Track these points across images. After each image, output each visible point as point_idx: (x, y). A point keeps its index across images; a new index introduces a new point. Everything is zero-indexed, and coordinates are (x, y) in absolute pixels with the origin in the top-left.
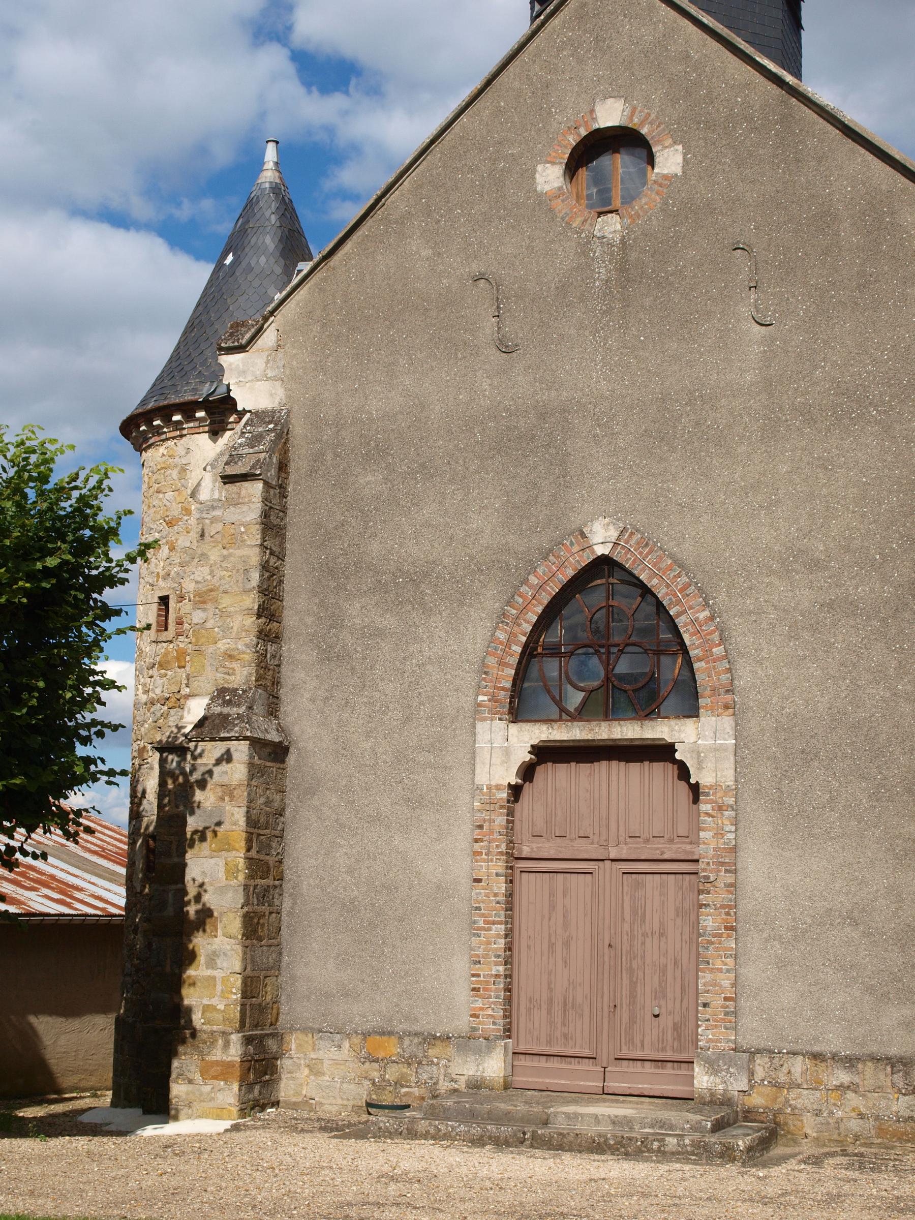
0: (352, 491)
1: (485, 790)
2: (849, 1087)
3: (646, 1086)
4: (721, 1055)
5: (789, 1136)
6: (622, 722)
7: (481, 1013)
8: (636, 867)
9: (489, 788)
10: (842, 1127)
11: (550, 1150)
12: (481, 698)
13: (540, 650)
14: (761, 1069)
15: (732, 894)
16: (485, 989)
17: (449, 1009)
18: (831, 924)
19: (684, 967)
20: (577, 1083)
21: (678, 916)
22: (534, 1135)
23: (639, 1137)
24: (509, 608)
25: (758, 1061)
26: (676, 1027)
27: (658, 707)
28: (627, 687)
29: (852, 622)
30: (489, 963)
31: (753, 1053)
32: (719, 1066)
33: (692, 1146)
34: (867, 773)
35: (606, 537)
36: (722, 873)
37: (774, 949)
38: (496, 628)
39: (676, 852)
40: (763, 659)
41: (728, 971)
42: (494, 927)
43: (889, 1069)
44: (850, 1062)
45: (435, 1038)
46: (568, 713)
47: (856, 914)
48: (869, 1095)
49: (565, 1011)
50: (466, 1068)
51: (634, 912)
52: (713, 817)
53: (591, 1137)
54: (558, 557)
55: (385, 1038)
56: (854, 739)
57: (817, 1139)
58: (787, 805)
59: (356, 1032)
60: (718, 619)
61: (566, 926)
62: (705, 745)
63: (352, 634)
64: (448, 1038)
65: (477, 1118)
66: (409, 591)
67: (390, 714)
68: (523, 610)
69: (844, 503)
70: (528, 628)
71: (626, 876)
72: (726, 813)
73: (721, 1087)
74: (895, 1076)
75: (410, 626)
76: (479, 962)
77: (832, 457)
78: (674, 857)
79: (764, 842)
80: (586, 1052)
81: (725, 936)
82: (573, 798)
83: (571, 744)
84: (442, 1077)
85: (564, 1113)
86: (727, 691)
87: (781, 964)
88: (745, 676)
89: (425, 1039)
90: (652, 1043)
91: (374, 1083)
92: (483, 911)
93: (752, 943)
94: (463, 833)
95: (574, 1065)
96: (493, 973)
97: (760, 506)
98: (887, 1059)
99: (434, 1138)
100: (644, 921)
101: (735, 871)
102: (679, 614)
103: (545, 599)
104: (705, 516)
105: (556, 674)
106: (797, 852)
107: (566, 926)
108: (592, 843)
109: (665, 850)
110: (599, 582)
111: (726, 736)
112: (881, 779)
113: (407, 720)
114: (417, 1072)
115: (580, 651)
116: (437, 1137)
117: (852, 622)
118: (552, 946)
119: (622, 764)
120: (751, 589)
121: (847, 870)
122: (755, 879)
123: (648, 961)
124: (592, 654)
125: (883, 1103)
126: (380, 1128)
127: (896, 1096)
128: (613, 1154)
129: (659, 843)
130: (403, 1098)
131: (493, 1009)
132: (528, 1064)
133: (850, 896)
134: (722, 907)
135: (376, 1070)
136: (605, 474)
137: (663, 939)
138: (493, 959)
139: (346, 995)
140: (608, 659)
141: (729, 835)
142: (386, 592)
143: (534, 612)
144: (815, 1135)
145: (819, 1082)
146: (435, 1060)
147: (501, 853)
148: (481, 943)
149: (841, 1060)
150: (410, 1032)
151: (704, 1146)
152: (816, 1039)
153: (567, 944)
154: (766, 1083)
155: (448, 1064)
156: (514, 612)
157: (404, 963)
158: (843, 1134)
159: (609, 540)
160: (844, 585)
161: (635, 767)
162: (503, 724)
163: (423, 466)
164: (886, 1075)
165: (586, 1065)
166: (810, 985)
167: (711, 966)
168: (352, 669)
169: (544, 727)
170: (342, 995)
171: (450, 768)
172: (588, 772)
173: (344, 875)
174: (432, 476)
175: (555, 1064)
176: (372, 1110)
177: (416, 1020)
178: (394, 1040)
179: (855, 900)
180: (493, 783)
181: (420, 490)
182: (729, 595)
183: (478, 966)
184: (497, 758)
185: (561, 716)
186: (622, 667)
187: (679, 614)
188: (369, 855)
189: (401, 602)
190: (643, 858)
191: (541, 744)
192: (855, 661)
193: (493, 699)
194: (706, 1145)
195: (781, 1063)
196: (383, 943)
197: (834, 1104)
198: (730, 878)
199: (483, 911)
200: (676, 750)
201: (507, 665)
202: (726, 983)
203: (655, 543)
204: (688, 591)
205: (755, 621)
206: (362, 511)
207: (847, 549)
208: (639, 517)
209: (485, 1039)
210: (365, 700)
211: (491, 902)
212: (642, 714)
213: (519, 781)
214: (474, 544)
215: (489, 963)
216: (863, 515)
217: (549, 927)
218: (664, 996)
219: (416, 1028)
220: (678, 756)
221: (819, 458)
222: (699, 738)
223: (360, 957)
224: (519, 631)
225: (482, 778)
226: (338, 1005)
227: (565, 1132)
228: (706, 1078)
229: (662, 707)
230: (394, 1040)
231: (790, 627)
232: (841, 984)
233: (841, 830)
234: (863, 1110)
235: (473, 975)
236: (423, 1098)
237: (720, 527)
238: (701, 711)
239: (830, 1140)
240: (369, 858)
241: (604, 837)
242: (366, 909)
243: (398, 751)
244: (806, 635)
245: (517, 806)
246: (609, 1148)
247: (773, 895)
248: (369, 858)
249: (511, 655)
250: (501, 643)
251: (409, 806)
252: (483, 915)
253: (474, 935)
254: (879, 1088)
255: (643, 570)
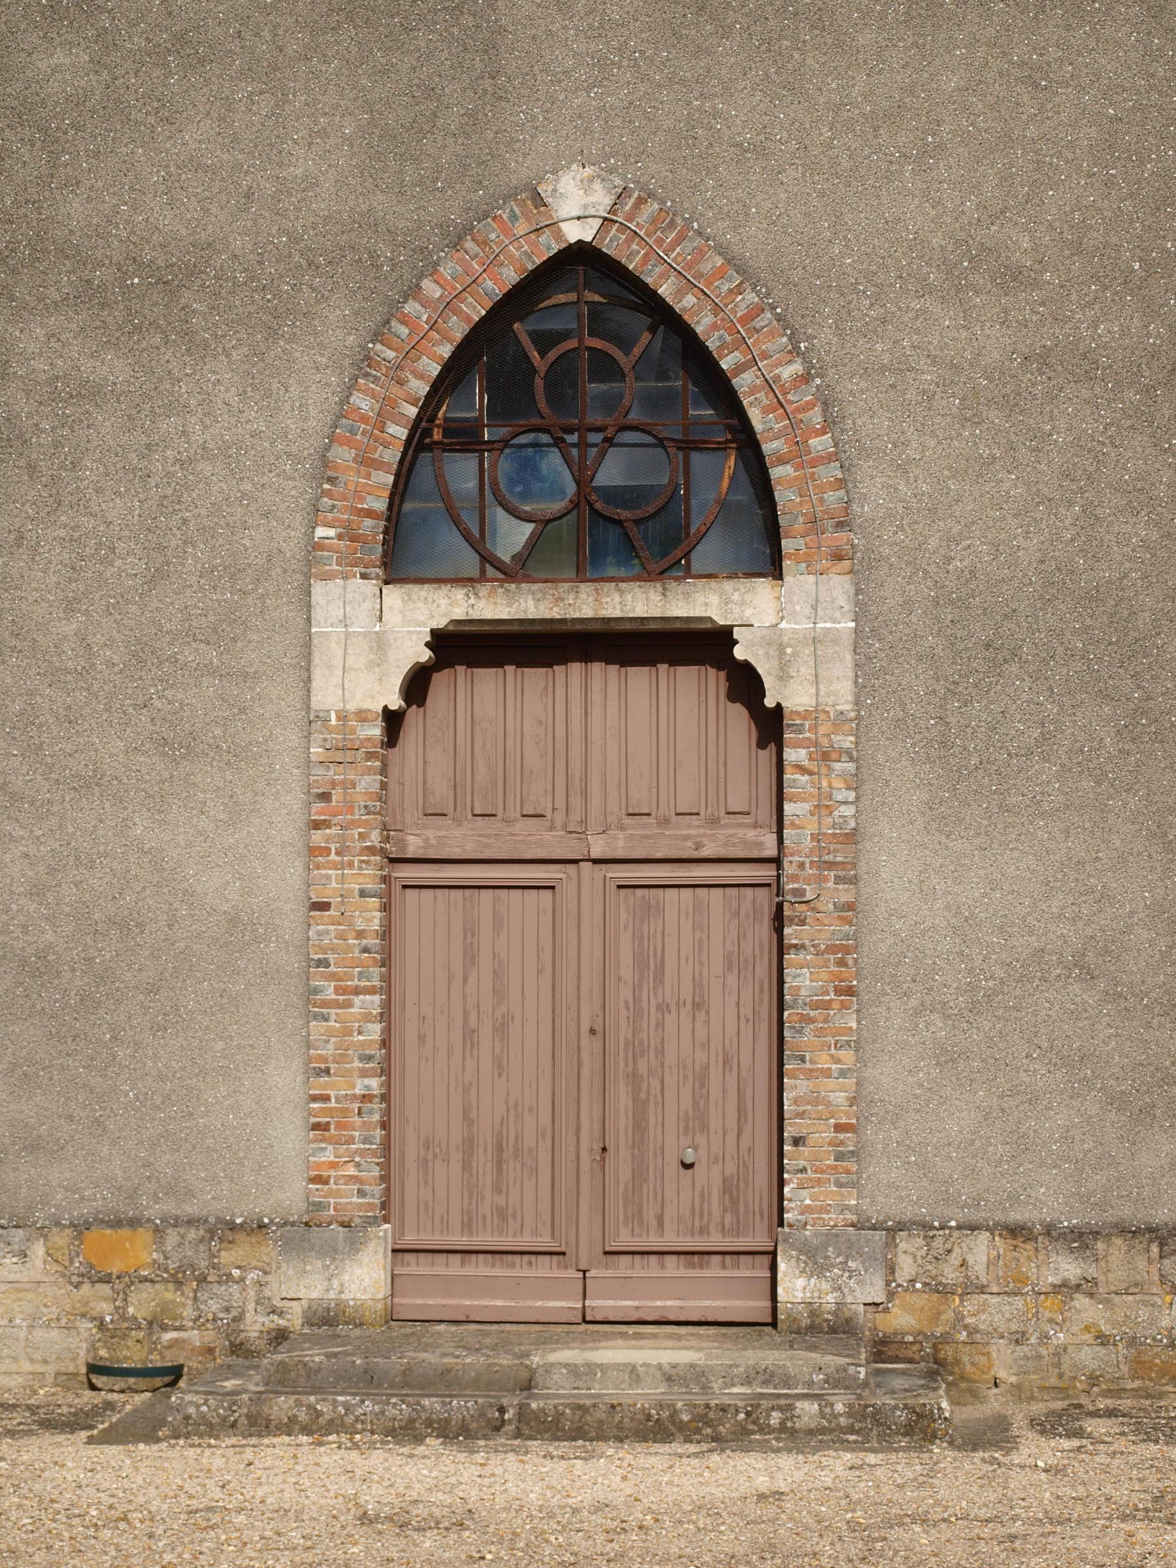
0: (19, 85)
1: (334, 722)
2: (1078, 1286)
3: (670, 1303)
4: (832, 1237)
5: (963, 1385)
6: (623, 585)
7: (333, 1173)
8: (641, 875)
9: (342, 716)
10: (1066, 1361)
11: (558, 1439)
12: (321, 532)
13: (437, 435)
14: (909, 1260)
15: (850, 924)
16: (340, 1126)
17: (261, 1167)
18: (1043, 979)
19: (744, 1072)
20: (529, 1303)
21: (730, 968)
22: (523, 1413)
23: (741, 1404)
24: (379, 347)
25: (903, 1246)
26: (728, 1187)
27: (687, 555)
28: (624, 514)
29: (1085, 394)
30: (348, 1073)
31: (894, 1230)
32: (827, 1257)
33: (849, 1415)
34: (1115, 687)
35: (585, 207)
36: (831, 884)
37: (932, 1029)
38: (351, 388)
39: (726, 845)
40: (909, 461)
41: (843, 1074)
42: (357, 1000)
43: (1155, 1249)
44: (1081, 1239)
45: (232, 1227)
46: (498, 566)
47: (1091, 957)
48: (1117, 1299)
49: (500, 1162)
50: (303, 1286)
51: (640, 962)
52: (811, 773)
53: (643, 1409)
54: (484, 243)
55: (125, 1232)
56: (1088, 622)
57: (1018, 1387)
58: (956, 750)
59: (58, 1224)
60: (818, 381)
61: (499, 994)
62: (795, 632)
63: (28, 393)
64: (261, 1226)
65: (380, 1386)
66: (156, 304)
67: (118, 563)
68: (412, 352)
69: (1070, 156)
70: (422, 389)
71: (623, 891)
72: (838, 766)
73: (831, 1298)
74: (1166, 1261)
75: (160, 380)
76: (327, 1071)
77: (1048, 64)
78: (723, 853)
79: (911, 822)
80: (544, 1241)
81: (836, 1005)
82: (510, 737)
83: (516, 628)
84: (250, 1306)
85: (566, 1366)
86: (840, 525)
87: (946, 1057)
88: (875, 494)
89: (212, 1232)
90: (680, 1219)
91: (102, 1326)
92: (332, 969)
93: (887, 1019)
94: (285, 811)
95: (521, 1269)
96: (358, 1091)
97: (903, 155)
98: (1150, 1230)
99: (307, 1430)
100: (662, 982)
101: (854, 881)
102: (740, 369)
103: (458, 330)
104: (790, 170)
105: (472, 484)
106: (978, 841)
107: (499, 994)
108: (552, 828)
109: (705, 841)
110: (562, 298)
111: (837, 614)
112: (1140, 700)
113: (158, 576)
114: (195, 1298)
115: (523, 439)
116: (316, 1428)
117: (1085, 394)
118: (470, 1035)
119: (613, 669)
120: (884, 321)
121: (1073, 875)
122: (893, 895)
123: (670, 1058)
124: (548, 445)
125: (1144, 1314)
126: (187, 1417)
127: (1168, 1298)
128: (688, 1440)
129: (689, 826)
130: (167, 1353)
131: (358, 1165)
132: (425, 1270)
133: (1080, 924)
134: (831, 949)
135: (105, 1299)
136: (581, 74)
137: (701, 1016)
138: (357, 1064)
139: (34, 1147)
140: (583, 457)
141: (843, 808)
142: (103, 306)
143: (433, 357)
144: (1013, 1379)
145: (1023, 1280)
146: (236, 1273)
147: (371, 850)
148: (330, 1033)
149: (1062, 1236)
150: (176, 1218)
151: (873, 1415)
152: (1014, 1199)
153: (501, 1029)
154: (919, 1286)
155: (264, 1279)
156: (391, 354)
157: (160, 1077)
158: (1068, 1374)
159: (592, 212)
160: (1070, 319)
161: (639, 676)
162: (371, 586)
163: (180, 38)
164: (1150, 1261)
165: (544, 1268)
166: (1001, 1097)
167: (808, 1065)
168: (29, 466)
169: (459, 594)
170: (25, 1148)
171: (256, 676)
172: (542, 684)
173: (23, 901)
174: (202, 62)
175: (479, 1268)
176: (98, 1380)
177: (190, 1193)
178: (144, 1235)
179: (1089, 932)
180: (351, 707)
181: (176, 89)
182: (840, 332)
183: (324, 1079)
184: (359, 659)
185: (483, 572)
186: (612, 472)
187: (740, 369)
188: (78, 858)
189: (138, 328)
190: (659, 855)
191: (451, 628)
192: (1092, 469)
193: (350, 534)
194: (878, 1411)
195: (948, 1246)
196: (114, 1038)
197: (1051, 1321)
198: (845, 894)
199: (332, 969)
200: (736, 642)
201: (378, 465)
202: (839, 1098)
203: (688, 222)
204: (759, 323)
205: (893, 386)
206: (44, 130)
207: (1077, 248)
208: (653, 167)
209: (343, 1225)
210: (62, 533)
211: (349, 949)
212: (655, 567)
213: (403, 703)
214: (299, 210)
215: (348, 1073)
216: (1109, 183)
217: (464, 997)
218: (704, 1127)
219: (190, 1209)
220: (739, 653)
221: (1022, 64)
222: (789, 622)
223: (62, 1068)
224: (401, 393)
225: (327, 695)
226: (15, 1170)
227: (588, 1402)
228: (801, 1282)
229: (693, 556)
230: (144, 1235)
231: (963, 399)
232: (1062, 1092)
233: (1061, 798)
234: (1105, 1328)
235: (314, 1098)
236: (211, 1351)
237: (822, 194)
238: (787, 563)
239: (1042, 1388)
240: (78, 863)
241: (576, 816)
242: (73, 970)
243: (139, 641)
244: (995, 416)
245: (394, 753)
246: (681, 1430)
247: (928, 924)
248: (78, 863)
249: (386, 445)
250: (364, 419)
251: (164, 754)
252: (333, 977)
253: (316, 1017)
254: (1136, 1285)
255: (664, 276)
